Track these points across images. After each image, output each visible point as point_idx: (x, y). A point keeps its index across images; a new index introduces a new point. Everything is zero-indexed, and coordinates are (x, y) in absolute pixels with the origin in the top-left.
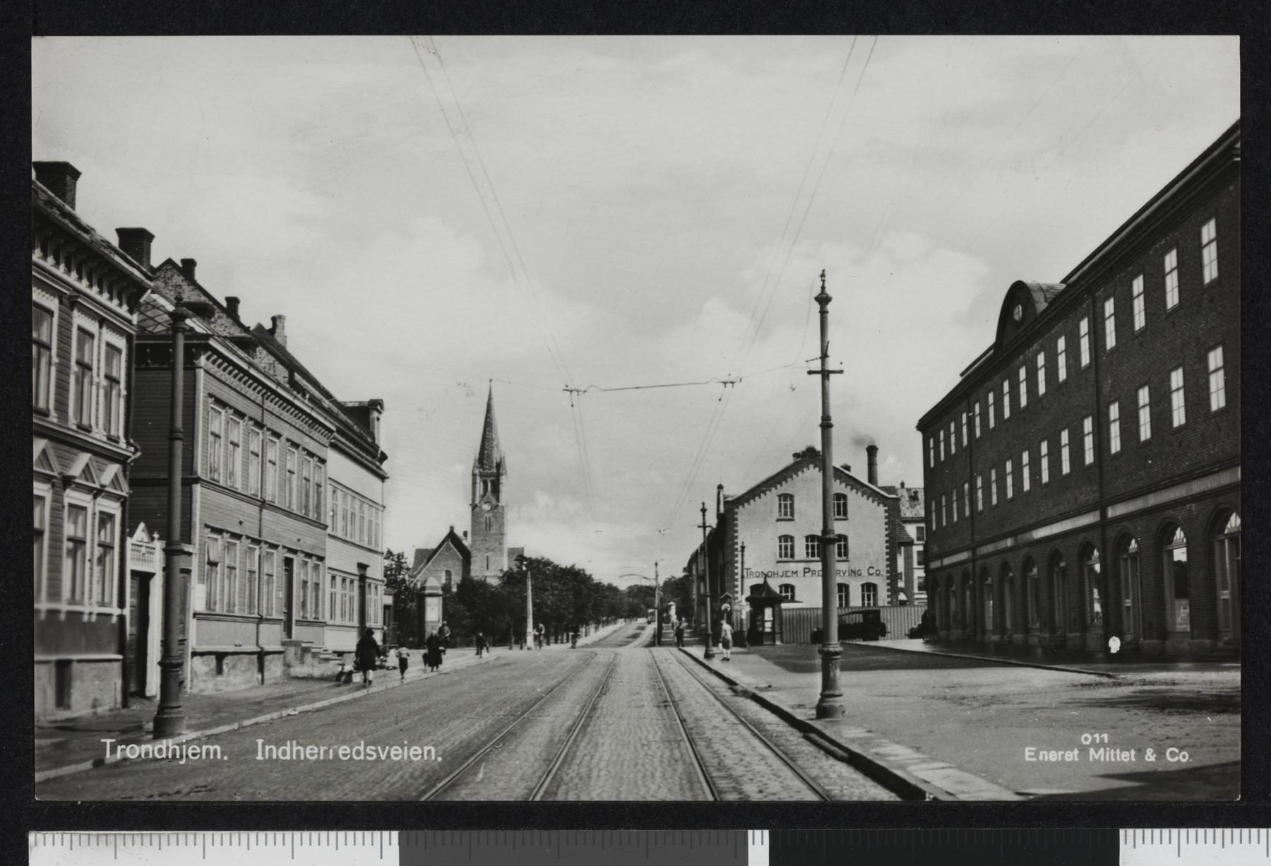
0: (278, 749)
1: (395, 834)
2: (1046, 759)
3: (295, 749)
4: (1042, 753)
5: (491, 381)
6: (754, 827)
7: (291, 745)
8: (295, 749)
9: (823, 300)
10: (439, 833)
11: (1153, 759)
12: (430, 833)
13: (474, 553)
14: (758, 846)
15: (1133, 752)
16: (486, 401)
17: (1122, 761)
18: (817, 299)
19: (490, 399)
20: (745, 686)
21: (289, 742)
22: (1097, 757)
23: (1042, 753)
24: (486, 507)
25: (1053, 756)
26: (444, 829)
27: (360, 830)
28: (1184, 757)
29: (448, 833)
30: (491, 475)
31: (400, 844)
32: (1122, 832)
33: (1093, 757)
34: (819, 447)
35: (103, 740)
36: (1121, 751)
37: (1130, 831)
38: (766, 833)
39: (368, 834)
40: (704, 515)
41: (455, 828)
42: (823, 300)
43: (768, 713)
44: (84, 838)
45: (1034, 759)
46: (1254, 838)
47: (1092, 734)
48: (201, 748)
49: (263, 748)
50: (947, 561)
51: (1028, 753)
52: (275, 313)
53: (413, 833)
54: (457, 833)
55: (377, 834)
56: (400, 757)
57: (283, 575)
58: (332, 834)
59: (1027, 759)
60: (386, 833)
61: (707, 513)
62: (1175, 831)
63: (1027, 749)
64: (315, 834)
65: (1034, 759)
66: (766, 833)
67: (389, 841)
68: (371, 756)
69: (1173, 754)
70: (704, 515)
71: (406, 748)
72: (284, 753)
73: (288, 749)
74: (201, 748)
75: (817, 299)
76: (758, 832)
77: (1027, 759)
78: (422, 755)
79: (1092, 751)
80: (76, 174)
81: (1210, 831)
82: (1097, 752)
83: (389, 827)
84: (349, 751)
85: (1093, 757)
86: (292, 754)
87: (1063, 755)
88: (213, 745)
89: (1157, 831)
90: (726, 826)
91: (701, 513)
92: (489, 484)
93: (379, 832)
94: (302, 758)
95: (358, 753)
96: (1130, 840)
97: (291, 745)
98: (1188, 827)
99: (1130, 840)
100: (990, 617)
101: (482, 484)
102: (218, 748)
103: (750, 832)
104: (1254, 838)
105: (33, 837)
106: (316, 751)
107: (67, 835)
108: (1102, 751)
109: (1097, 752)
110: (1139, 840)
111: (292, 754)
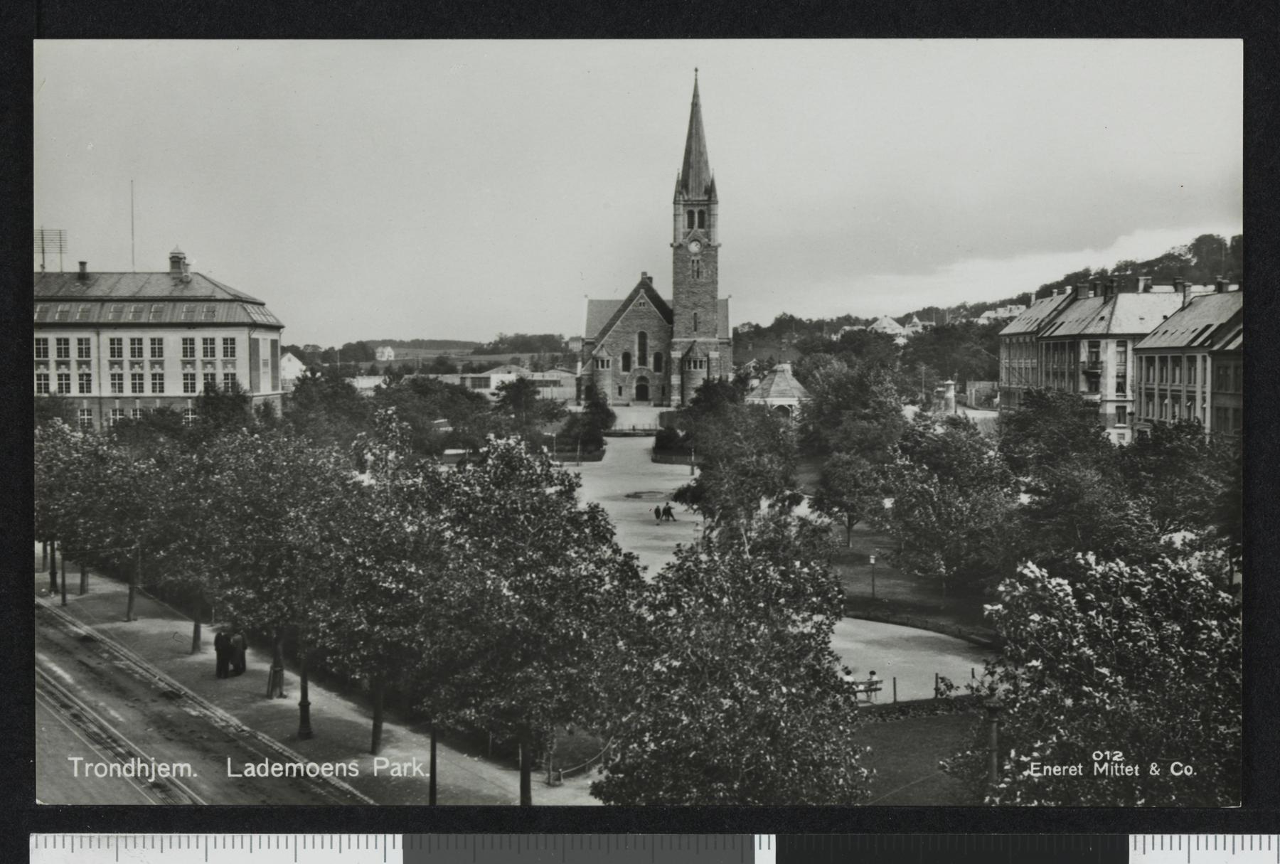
1: (399, 837)
3: (140, 766)
4: (1045, 768)
5: (696, 70)
6: (761, 832)
10: (443, 837)
12: (434, 836)
13: (678, 310)
14: (765, 851)
16: (690, 100)
19: (696, 95)
22: (1101, 771)
23: (1045, 768)
24: (694, 247)
26: (448, 832)
27: (363, 833)
28: (1189, 770)
29: (452, 836)
30: (698, 203)
31: (404, 847)
32: (1131, 837)
33: (1098, 771)
37: (1140, 837)
38: (773, 837)
39: (372, 837)
41: (459, 831)
47: (1103, 752)
48: (334, 765)
53: (416, 836)
54: (461, 837)
55: (381, 837)
58: (336, 837)
60: (390, 837)
62: (1185, 837)
66: (773, 837)
68: (354, 772)
73: (132, 766)
74: (334, 765)
76: (764, 837)
83: (394, 831)
85: (1098, 771)
86: (136, 771)
87: (1067, 771)
89: (1167, 837)
90: (733, 831)
92: (696, 216)
93: (383, 836)
95: (129, 771)
96: (1140, 845)
98: (1198, 833)
99: (1140, 845)
101: (686, 216)
103: (757, 837)
105: (33, 838)
106: (281, 768)
107: (68, 837)
110: (1149, 846)
111: (136, 771)
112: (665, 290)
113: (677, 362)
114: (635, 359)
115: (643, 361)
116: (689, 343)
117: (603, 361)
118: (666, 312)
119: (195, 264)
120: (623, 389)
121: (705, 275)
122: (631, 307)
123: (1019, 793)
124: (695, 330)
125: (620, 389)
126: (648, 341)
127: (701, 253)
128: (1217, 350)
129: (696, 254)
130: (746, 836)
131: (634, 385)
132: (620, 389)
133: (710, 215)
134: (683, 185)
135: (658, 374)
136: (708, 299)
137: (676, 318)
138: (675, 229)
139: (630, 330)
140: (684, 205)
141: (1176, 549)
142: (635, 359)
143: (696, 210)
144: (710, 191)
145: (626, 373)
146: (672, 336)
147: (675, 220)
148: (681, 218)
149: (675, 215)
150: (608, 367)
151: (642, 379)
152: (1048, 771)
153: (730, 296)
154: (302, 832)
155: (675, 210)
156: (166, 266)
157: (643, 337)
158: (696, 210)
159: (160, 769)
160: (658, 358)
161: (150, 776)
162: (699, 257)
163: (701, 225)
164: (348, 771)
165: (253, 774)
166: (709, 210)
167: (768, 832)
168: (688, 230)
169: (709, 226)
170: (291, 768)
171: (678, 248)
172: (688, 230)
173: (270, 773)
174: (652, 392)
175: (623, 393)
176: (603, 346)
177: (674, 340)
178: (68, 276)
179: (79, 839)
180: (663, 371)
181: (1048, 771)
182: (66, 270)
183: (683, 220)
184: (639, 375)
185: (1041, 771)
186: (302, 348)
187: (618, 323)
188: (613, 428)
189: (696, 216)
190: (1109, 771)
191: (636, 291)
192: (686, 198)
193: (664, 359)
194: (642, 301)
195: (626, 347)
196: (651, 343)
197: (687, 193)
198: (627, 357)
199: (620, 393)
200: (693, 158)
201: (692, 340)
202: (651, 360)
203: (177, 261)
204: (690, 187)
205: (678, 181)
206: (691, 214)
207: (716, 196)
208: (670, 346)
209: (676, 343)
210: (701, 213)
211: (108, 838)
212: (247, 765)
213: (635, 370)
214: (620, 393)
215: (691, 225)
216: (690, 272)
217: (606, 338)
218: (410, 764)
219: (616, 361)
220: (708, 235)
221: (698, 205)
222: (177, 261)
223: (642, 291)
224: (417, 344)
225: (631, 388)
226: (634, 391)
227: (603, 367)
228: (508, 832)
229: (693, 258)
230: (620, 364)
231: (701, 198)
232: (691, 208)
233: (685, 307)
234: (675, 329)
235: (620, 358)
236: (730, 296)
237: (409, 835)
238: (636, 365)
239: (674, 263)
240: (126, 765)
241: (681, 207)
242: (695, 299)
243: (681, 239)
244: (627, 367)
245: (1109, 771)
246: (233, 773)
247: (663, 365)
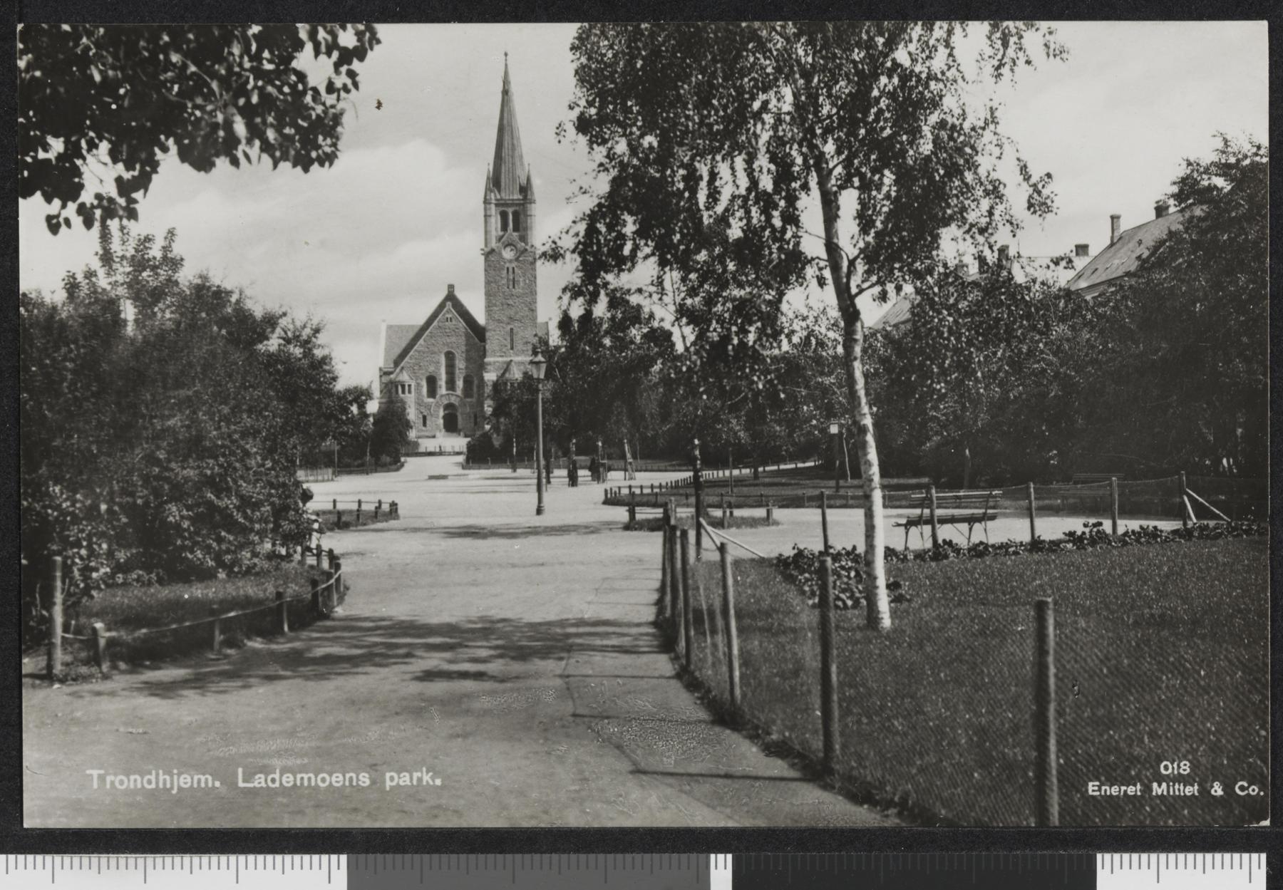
1: (344, 858)
2: (1108, 793)
4: (1103, 788)
7: (157, 775)
8: (161, 778)
11: (1220, 793)
14: (721, 870)
15: (1139, 787)
17: (268, 787)
21: (154, 772)
23: (1103, 788)
24: (508, 254)
25: (1114, 791)
32: (1099, 856)
35: (88, 772)
36: (1185, 786)
37: (1107, 856)
38: (729, 856)
44: (141, 861)
45: (1098, 793)
46: (30, 864)
53: (362, 857)
56: (341, 783)
57: (627, 674)
59: (1090, 793)
60: (334, 857)
62: (1246, 856)
63: (1090, 784)
64: (76, 858)
65: (1098, 793)
66: (729, 856)
67: (338, 865)
69: (1242, 788)
71: (175, 777)
72: (149, 782)
73: (153, 777)
76: (721, 857)
77: (1090, 793)
79: (1155, 785)
81: (270, 857)
82: (1160, 786)
86: (157, 783)
88: (307, 773)
97: (157, 775)
101: (499, 217)
102: (1090, 784)
103: (713, 856)
104: (30, 864)
106: (341, 778)
107: (94, 858)
108: (1164, 785)
109: (1160, 786)
112: (477, 307)
113: (490, 384)
114: (442, 382)
115: (451, 384)
116: (505, 362)
117: (403, 387)
118: (477, 332)
120: (428, 418)
121: (522, 284)
122: (435, 323)
124: (512, 348)
125: (425, 418)
126: (457, 362)
127: (517, 259)
128: (143, 627)
129: (510, 261)
130: (702, 856)
131: (441, 413)
132: (425, 418)
133: (527, 216)
134: (495, 181)
135: (469, 400)
136: (526, 311)
137: (488, 334)
138: (486, 232)
139: (436, 349)
140: (497, 205)
142: (442, 382)
143: (510, 211)
144: (525, 190)
145: (431, 400)
146: (484, 356)
147: (486, 222)
148: (493, 220)
149: (486, 216)
150: (410, 392)
151: (449, 407)
152: (1106, 791)
154: (234, 853)
155: (485, 209)
157: (450, 357)
158: (510, 211)
160: (468, 382)
162: (514, 265)
163: (516, 229)
165: (263, 785)
166: (525, 210)
167: (1259, 850)
168: (501, 233)
169: (526, 229)
170: (302, 779)
171: (489, 254)
172: (501, 233)
173: (281, 784)
174: (461, 422)
175: (428, 422)
176: (403, 368)
177: (487, 360)
179: (69, 859)
180: (476, 395)
181: (1106, 791)
183: (496, 221)
184: (446, 402)
185: (1100, 790)
187: (421, 341)
189: (511, 217)
190: (1168, 791)
191: (441, 306)
192: (498, 197)
193: (476, 382)
194: (449, 316)
195: (432, 369)
196: (460, 364)
197: (499, 192)
198: (432, 382)
199: (425, 424)
201: (509, 359)
202: (460, 384)
204: (503, 184)
205: (488, 178)
206: (504, 216)
207: (532, 194)
208: (482, 367)
209: (489, 364)
210: (516, 214)
211: (136, 858)
213: (442, 396)
214: (425, 424)
215: (504, 227)
216: (504, 281)
217: (407, 359)
218: (419, 774)
219: (418, 385)
220: (523, 239)
221: (512, 205)
223: (449, 304)
225: (437, 417)
226: (441, 421)
227: (403, 392)
228: (624, 851)
229: (507, 265)
230: (425, 390)
231: (515, 197)
232: (505, 209)
233: (499, 321)
234: (487, 347)
235: (424, 383)
237: (354, 856)
238: (442, 390)
239: (486, 270)
241: (493, 206)
242: (512, 312)
243: (494, 244)
244: (432, 392)
245: (1168, 791)
246: (244, 781)
247: (475, 389)
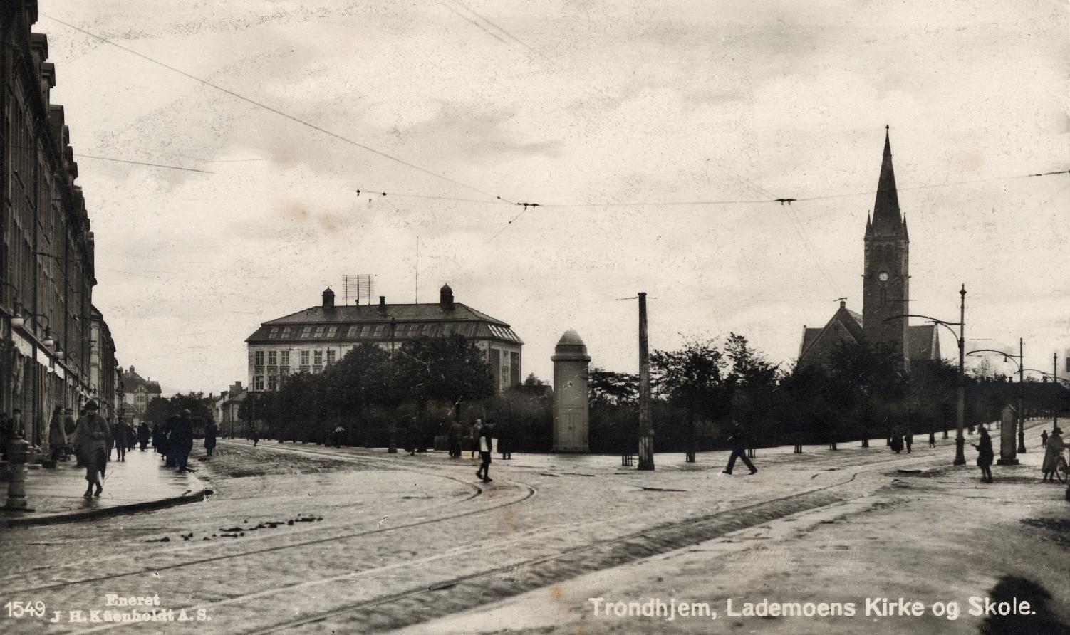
0: (802, 606)
9: (963, 292)
18: (960, 292)
20: (65, 479)
34: (31, 356)
40: (963, 298)
42: (963, 292)
43: (58, 526)
49: (888, 606)
50: (11, 403)
51: (737, 424)
52: (642, 291)
61: (966, 295)
70: (963, 298)
75: (960, 292)
78: (690, 611)
80: (96, 283)
84: (688, 608)
91: (960, 295)
94: (1015, 613)
100: (505, 369)
119: (458, 298)
123: (904, 437)
141: (402, 345)
153: (963, 285)
156: (436, 299)
159: (680, 609)
161: (669, 615)
164: (844, 610)
178: (91, 263)
182: (349, 304)
186: (455, 300)
188: (14, 332)
200: (439, 587)
203: (446, 293)
212: (746, 605)
218: (896, 604)
222: (446, 293)
224: (510, 604)
236: (963, 285)
240: (646, 604)
